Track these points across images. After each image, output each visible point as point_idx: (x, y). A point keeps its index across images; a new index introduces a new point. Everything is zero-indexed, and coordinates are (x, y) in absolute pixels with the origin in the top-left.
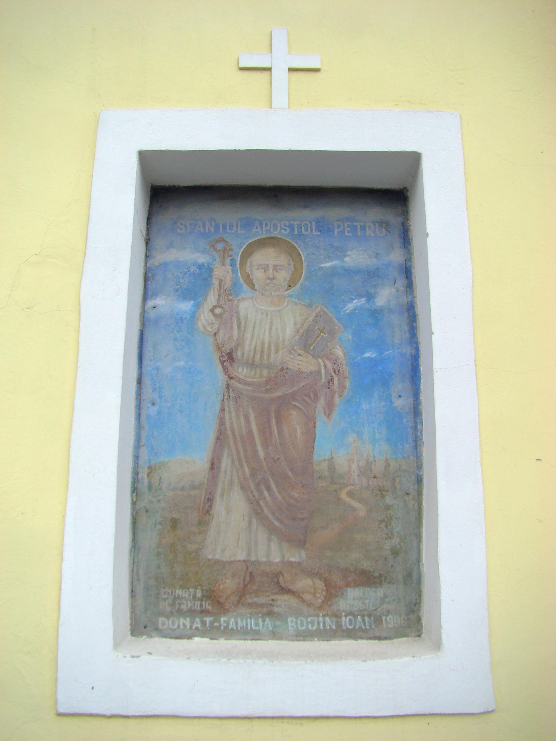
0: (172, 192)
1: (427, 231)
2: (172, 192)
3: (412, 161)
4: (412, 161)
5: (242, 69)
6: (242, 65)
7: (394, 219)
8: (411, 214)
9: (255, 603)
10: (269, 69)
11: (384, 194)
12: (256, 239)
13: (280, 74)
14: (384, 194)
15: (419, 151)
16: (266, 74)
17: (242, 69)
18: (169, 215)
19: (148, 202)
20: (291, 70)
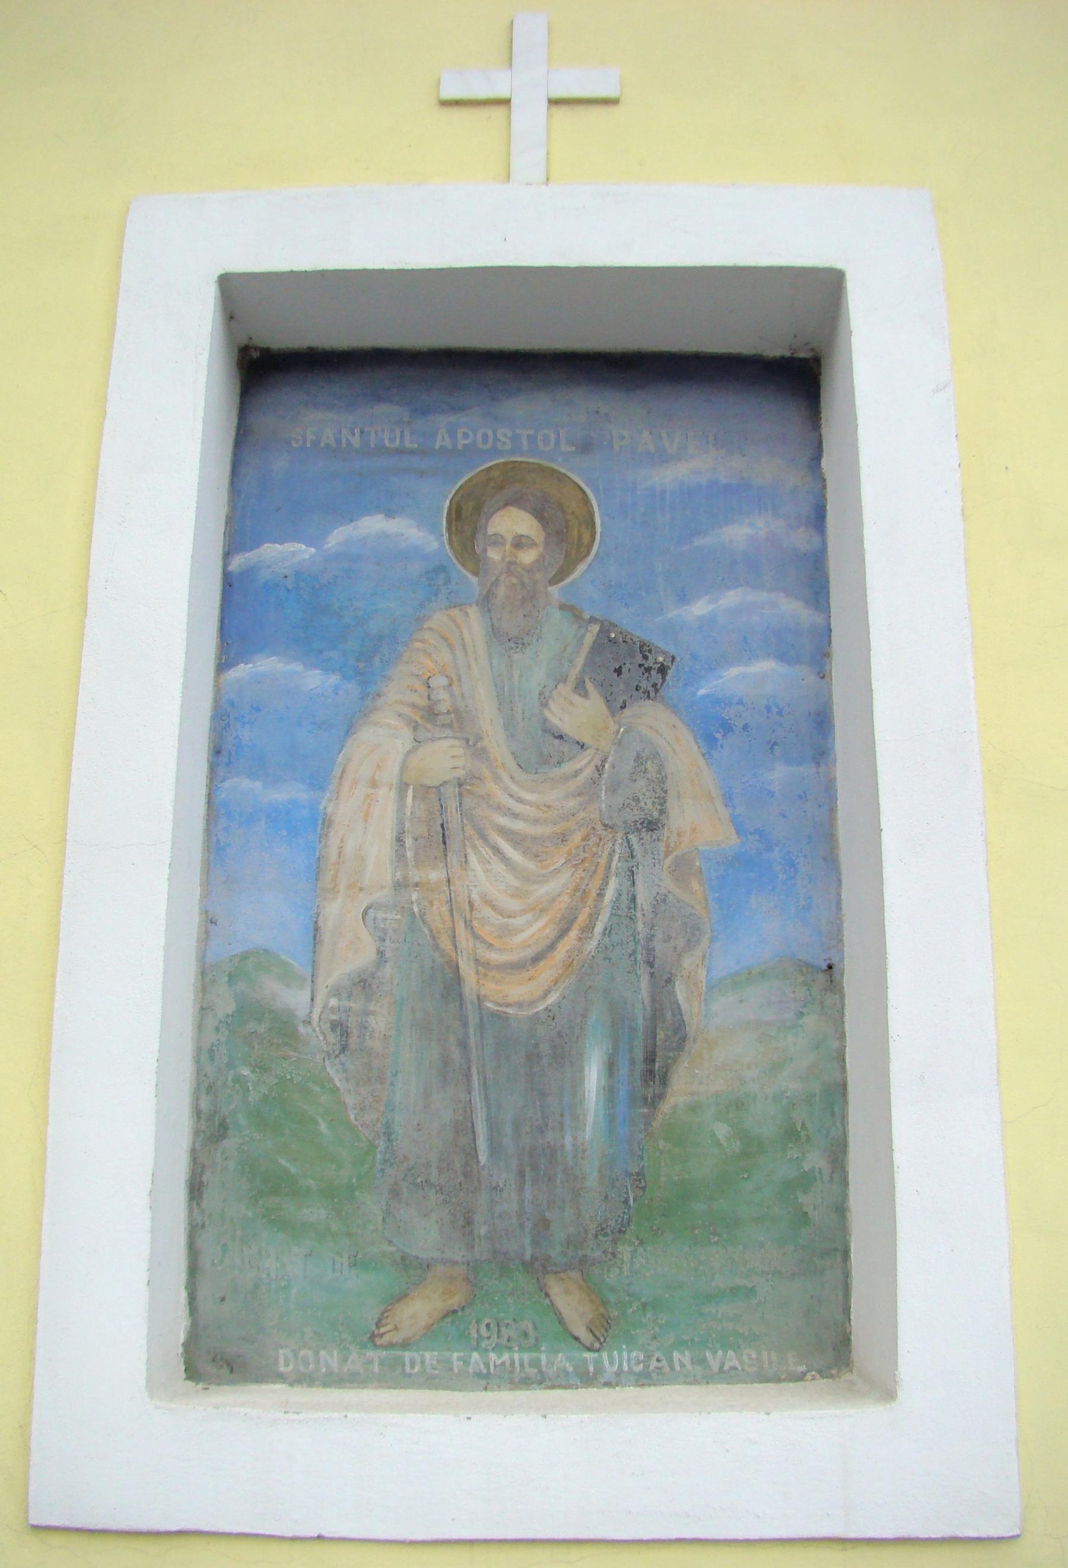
0: (285, 363)
1: (155, 1100)
2: (285, 363)
3: (825, 289)
4: (825, 289)
5: (446, 104)
6: (448, 94)
7: (769, 467)
8: (822, 405)
9: (524, 1183)
10: (506, 102)
11: (768, 368)
12: (503, 460)
13: (531, 113)
14: (768, 368)
15: (839, 266)
16: (498, 112)
17: (446, 104)
18: (316, 422)
19: (238, 389)
20: (554, 102)
